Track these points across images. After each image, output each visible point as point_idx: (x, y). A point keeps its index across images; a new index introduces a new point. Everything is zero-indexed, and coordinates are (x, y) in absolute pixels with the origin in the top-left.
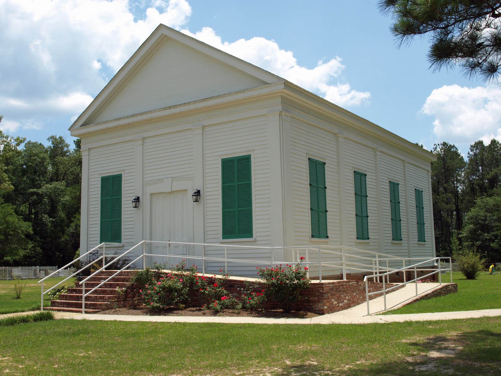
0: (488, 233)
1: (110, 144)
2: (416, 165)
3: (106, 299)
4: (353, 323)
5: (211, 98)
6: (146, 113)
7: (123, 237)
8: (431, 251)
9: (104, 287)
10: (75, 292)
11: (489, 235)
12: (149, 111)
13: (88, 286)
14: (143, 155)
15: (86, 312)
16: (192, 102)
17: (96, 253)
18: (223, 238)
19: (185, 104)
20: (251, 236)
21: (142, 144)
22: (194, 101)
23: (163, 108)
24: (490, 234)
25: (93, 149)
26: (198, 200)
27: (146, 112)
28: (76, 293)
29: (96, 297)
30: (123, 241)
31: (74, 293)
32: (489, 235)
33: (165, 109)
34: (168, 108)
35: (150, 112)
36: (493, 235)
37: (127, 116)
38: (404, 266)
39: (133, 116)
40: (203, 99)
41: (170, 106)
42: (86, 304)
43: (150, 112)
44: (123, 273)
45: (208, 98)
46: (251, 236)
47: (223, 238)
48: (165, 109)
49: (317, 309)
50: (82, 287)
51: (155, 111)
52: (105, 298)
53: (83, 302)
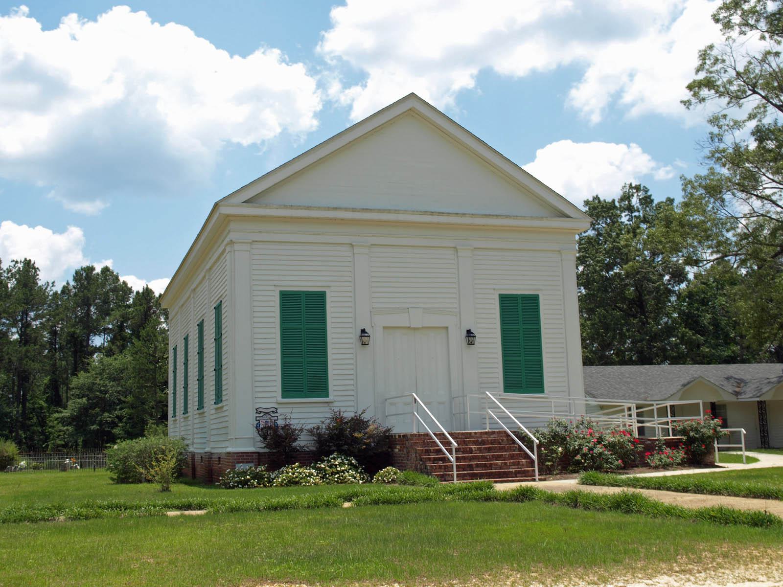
0: (109, 412)
3: (523, 465)
4: (775, 466)
6: (389, 211)
7: (331, 387)
9: (478, 452)
11: (111, 416)
14: (459, 279)
15: (540, 480)
16: (469, 214)
18: (283, 397)
19: (457, 214)
20: (542, 391)
21: (355, 255)
22: (472, 214)
23: (421, 212)
24: (113, 415)
25: (256, 243)
32: (111, 416)
33: (425, 213)
34: (429, 213)
35: (396, 211)
36: (117, 417)
37: (353, 209)
40: (486, 215)
41: (433, 211)
42: (458, 476)
43: (396, 211)
44: (473, 434)
45: (493, 215)
46: (542, 391)
47: (283, 397)
48: (425, 213)
49: (709, 461)
51: (405, 212)
52: (521, 463)
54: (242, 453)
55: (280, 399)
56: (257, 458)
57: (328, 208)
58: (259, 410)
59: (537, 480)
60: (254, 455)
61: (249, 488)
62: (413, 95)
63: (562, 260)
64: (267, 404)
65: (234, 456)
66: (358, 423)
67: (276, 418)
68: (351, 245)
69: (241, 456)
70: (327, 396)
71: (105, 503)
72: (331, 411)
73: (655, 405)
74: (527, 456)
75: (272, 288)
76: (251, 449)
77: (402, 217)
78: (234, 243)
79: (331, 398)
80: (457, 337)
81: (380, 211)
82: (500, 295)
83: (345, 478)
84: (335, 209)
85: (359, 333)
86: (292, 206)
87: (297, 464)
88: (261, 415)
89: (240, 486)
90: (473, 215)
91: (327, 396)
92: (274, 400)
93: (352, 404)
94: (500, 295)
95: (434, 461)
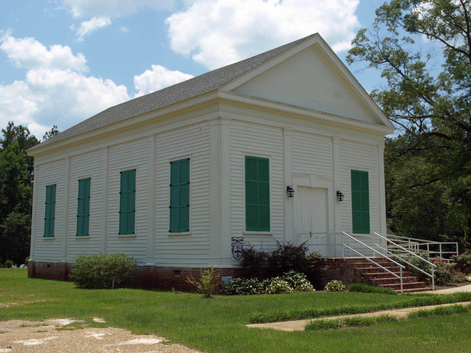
1: (299, 130)
2: (57, 159)
3: (414, 280)
5: (355, 120)
6: (306, 109)
7: (271, 225)
8: (36, 249)
10: (376, 277)
12: (309, 109)
13: (373, 272)
17: (241, 240)
18: (247, 230)
19: (337, 116)
23: (321, 112)
26: (342, 200)
27: (306, 108)
28: (377, 278)
29: (408, 278)
30: (272, 229)
31: (376, 278)
33: (322, 113)
37: (288, 105)
38: (374, 255)
39: (297, 107)
40: (350, 118)
44: (334, 260)
47: (247, 230)
48: (322, 113)
50: (400, 271)
52: (414, 279)
53: (402, 284)
54: (226, 269)
55: (245, 231)
56: (235, 273)
57: (276, 102)
58: (234, 238)
59: (434, 289)
60: (232, 270)
61: (251, 294)
62: (317, 34)
63: (378, 152)
64: (238, 235)
65: (221, 271)
66: (301, 250)
67: (242, 244)
68: (283, 129)
69: (224, 271)
70: (269, 231)
71: (33, 302)
72: (274, 240)
73: (409, 240)
74: (428, 277)
75: (241, 153)
76: (230, 266)
77: (312, 114)
78: (221, 118)
79: (271, 232)
80: (332, 195)
81: (301, 108)
82: (246, 156)
83: (306, 288)
84: (279, 103)
85: (286, 189)
86: (257, 98)
87: (277, 277)
88: (234, 242)
89: (244, 293)
90: (344, 118)
91: (269, 231)
92: (241, 232)
93: (281, 236)
94: (246, 156)
95: (373, 277)
